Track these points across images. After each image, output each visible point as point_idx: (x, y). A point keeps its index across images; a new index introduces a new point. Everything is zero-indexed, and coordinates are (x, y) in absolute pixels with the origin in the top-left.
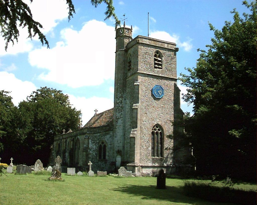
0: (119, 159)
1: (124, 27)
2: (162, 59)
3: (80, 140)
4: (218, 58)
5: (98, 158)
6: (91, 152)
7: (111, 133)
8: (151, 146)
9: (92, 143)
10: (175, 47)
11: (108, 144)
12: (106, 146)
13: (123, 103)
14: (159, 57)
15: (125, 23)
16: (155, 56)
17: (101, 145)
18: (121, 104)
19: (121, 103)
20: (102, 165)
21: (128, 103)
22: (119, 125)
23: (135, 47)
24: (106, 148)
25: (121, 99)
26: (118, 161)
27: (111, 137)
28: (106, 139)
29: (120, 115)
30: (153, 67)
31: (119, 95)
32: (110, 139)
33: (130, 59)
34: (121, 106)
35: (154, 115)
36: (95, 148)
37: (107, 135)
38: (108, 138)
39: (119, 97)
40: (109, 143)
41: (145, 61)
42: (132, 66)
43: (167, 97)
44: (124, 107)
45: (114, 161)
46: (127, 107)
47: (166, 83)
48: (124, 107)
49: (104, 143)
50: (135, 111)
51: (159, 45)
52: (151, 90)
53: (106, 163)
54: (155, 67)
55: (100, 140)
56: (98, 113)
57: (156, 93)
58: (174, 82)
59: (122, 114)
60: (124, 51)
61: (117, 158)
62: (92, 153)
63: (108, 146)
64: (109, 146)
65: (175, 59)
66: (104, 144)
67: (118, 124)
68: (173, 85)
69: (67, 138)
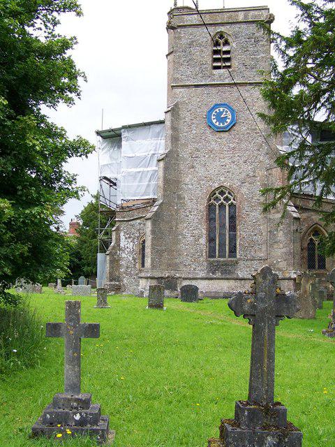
4: (320, 25)
6: (124, 255)
8: (204, 236)
9: (126, 238)
10: (265, 13)
30: (210, 67)
35: (214, 167)
51: (191, 21)
54: (216, 68)
55: (141, 231)
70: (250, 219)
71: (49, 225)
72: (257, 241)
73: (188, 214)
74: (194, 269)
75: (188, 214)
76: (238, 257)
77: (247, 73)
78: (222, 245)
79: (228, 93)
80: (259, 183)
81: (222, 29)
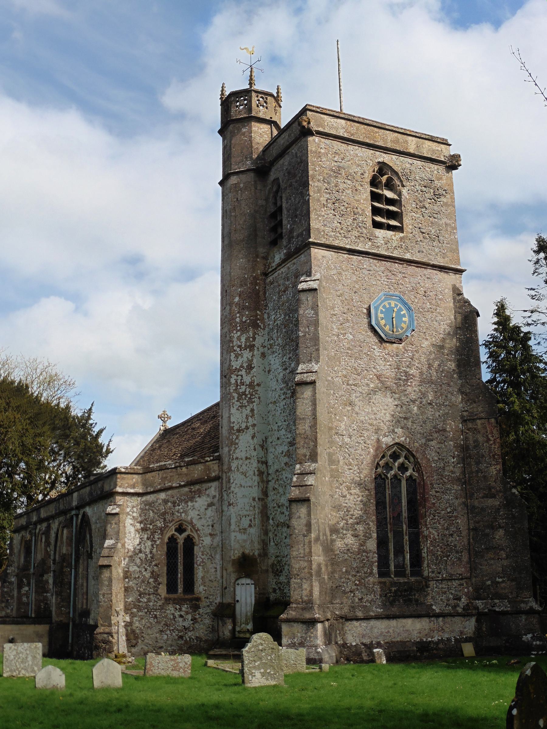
0: (245, 595)
1: (248, 87)
2: (400, 194)
3: (93, 520)
5: (163, 590)
7: (213, 489)
8: (375, 535)
11: (201, 533)
12: (196, 540)
13: (254, 370)
14: (389, 185)
15: (253, 74)
16: (374, 182)
17: (172, 540)
18: (248, 373)
19: (250, 367)
20: (181, 616)
21: (273, 367)
22: (243, 455)
23: (294, 150)
24: (195, 548)
25: (247, 354)
26: (243, 600)
27: (210, 505)
28: (192, 515)
29: (247, 418)
30: (369, 223)
31: (239, 339)
32: (209, 512)
33: (275, 204)
34: (248, 383)
36: (148, 550)
37: (197, 499)
38: (202, 510)
39: (240, 347)
40: (209, 530)
41: (336, 197)
42: (287, 225)
43: (427, 339)
44: (258, 385)
45: (228, 600)
46: (273, 384)
47: (422, 284)
48: (258, 385)
49: (185, 530)
50: (307, 392)
51: (332, 127)
52: (365, 311)
53: (196, 608)
54: (377, 225)
55: (168, 517)
56: (170, 424)
57: (383, 322)
58: (450, 279)
59: (252, 410)
60: (252, 175)
61: (238, 588)
62: (138, 569)
63: (204, 542)
64: (207, 541)
65: (448, 196)
66: (184, 535)
67: (237, 451)
68: (449, 292)
69: (53, 517)
70: (443, 506)
71: (70, 476)
72: (455, 546)
73: (345, 492)
74: (361, 599)
75: (345, 492)
76: (426, 574)
77: (425, 245)
78: (399, 551)
79: (400, 276)
80: (451, 443)
81: (386, 158)
